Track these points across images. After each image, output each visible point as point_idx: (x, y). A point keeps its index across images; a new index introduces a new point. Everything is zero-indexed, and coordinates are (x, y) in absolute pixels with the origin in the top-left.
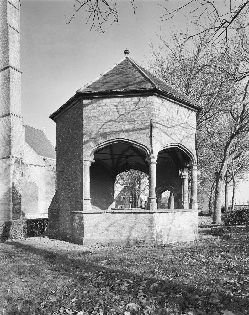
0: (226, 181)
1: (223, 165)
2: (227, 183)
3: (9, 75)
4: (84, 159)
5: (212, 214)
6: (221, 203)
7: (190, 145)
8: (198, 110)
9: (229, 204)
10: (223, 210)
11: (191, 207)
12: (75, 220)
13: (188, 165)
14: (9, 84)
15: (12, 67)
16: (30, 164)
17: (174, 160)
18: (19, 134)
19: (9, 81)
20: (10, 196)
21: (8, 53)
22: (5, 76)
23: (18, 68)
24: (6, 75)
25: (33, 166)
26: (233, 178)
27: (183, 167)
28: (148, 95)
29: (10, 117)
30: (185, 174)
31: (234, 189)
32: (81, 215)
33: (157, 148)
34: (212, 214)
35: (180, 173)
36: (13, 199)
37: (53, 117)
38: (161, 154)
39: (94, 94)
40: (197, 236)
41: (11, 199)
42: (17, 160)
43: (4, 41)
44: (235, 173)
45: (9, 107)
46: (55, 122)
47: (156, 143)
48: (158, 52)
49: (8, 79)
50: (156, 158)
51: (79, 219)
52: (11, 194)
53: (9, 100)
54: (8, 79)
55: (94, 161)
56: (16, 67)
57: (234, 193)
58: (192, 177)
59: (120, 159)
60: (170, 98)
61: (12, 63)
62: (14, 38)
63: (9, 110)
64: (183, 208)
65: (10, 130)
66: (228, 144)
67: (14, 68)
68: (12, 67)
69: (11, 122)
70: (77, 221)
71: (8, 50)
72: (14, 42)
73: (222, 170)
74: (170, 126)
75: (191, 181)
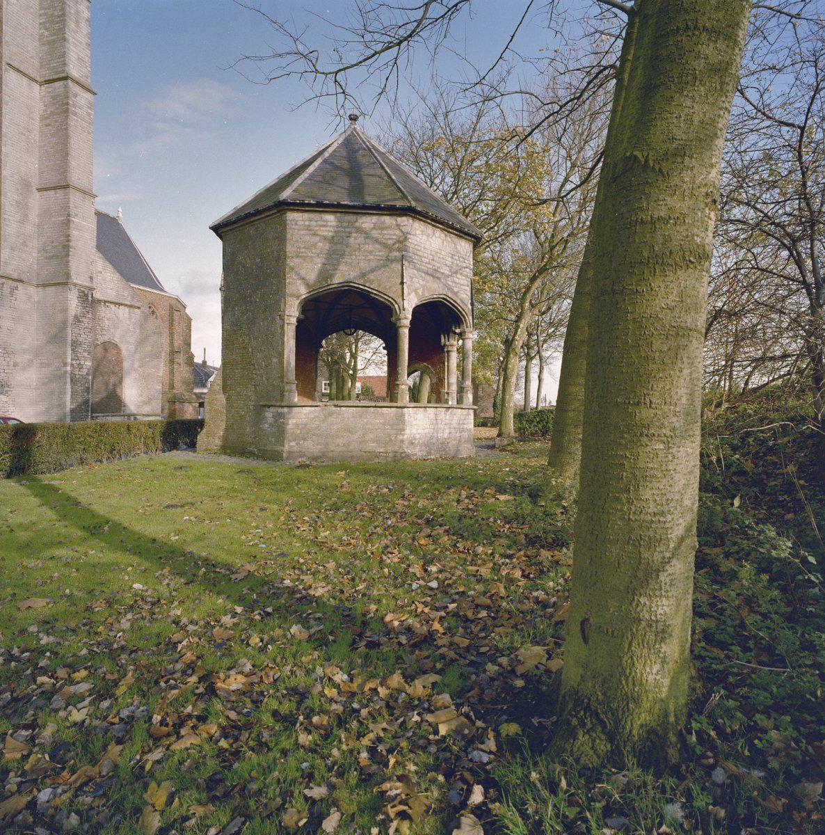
0: (528, 355)
1: (518, 327)
2: (529, 358)
3: (67, 97)
4: (287, 313)
5: (497, 423)
6: (517, 397)
7: (461, 293)
8: (476, 241)
9: (533, 404)
10: (520, 416)
11: (460, 401)
12: (264, 418)
13: (458, 331)
14: (67, 117)
15: (73, 80)
16: (105, 302)
17: (437, 320)
18: (85, 234)
19: (67, 111)
20: (66, 372)
21: (64, 47)
22: (54, 98)
23: (88, 82)
24: (57, 96)
25: (112, 306)
26: (539, 352)
27: (448, 332)
28: (400, 215)
29: (66, 194)
30: (454, 343)
31: (541, 372)
32: (280, 410)
33: (409, 304)
34: (497, 423)
35: (443, 340)
36: (72, 380)
37: (217, 229)
38: (417, 311)
39: (309, 205)
40: (473, 452)
41: (69, 380)
42: (83, 292)
43: (52, 15)
44: (545, 341)
45: (66, 171)
46: (221, 238)
47: (409, 294)
48: (407, 112)
49: (63, 104)
50: (410, 317)
51: (274, 417)
52: (69, 368)
53: (67, 154)
54: (63, 104)
55: (302, 317)
56: (82, 80)
57: (540, 381)
58: (464, 346)
59: (344, 311)
60: (432, 220)
61: (74, 71)
62: (78, 12)
63: (66, 177)
64: (447, 401)
65: (67, 223)
66: (528, 289)
67: (78, 83)
68: (73, 80)
69: (71, 205)
70: (271, 420)
71: (65, 39)
72: (77, 22)
73: (517, 337)
74: (431, 264)
75: (462, 351)
